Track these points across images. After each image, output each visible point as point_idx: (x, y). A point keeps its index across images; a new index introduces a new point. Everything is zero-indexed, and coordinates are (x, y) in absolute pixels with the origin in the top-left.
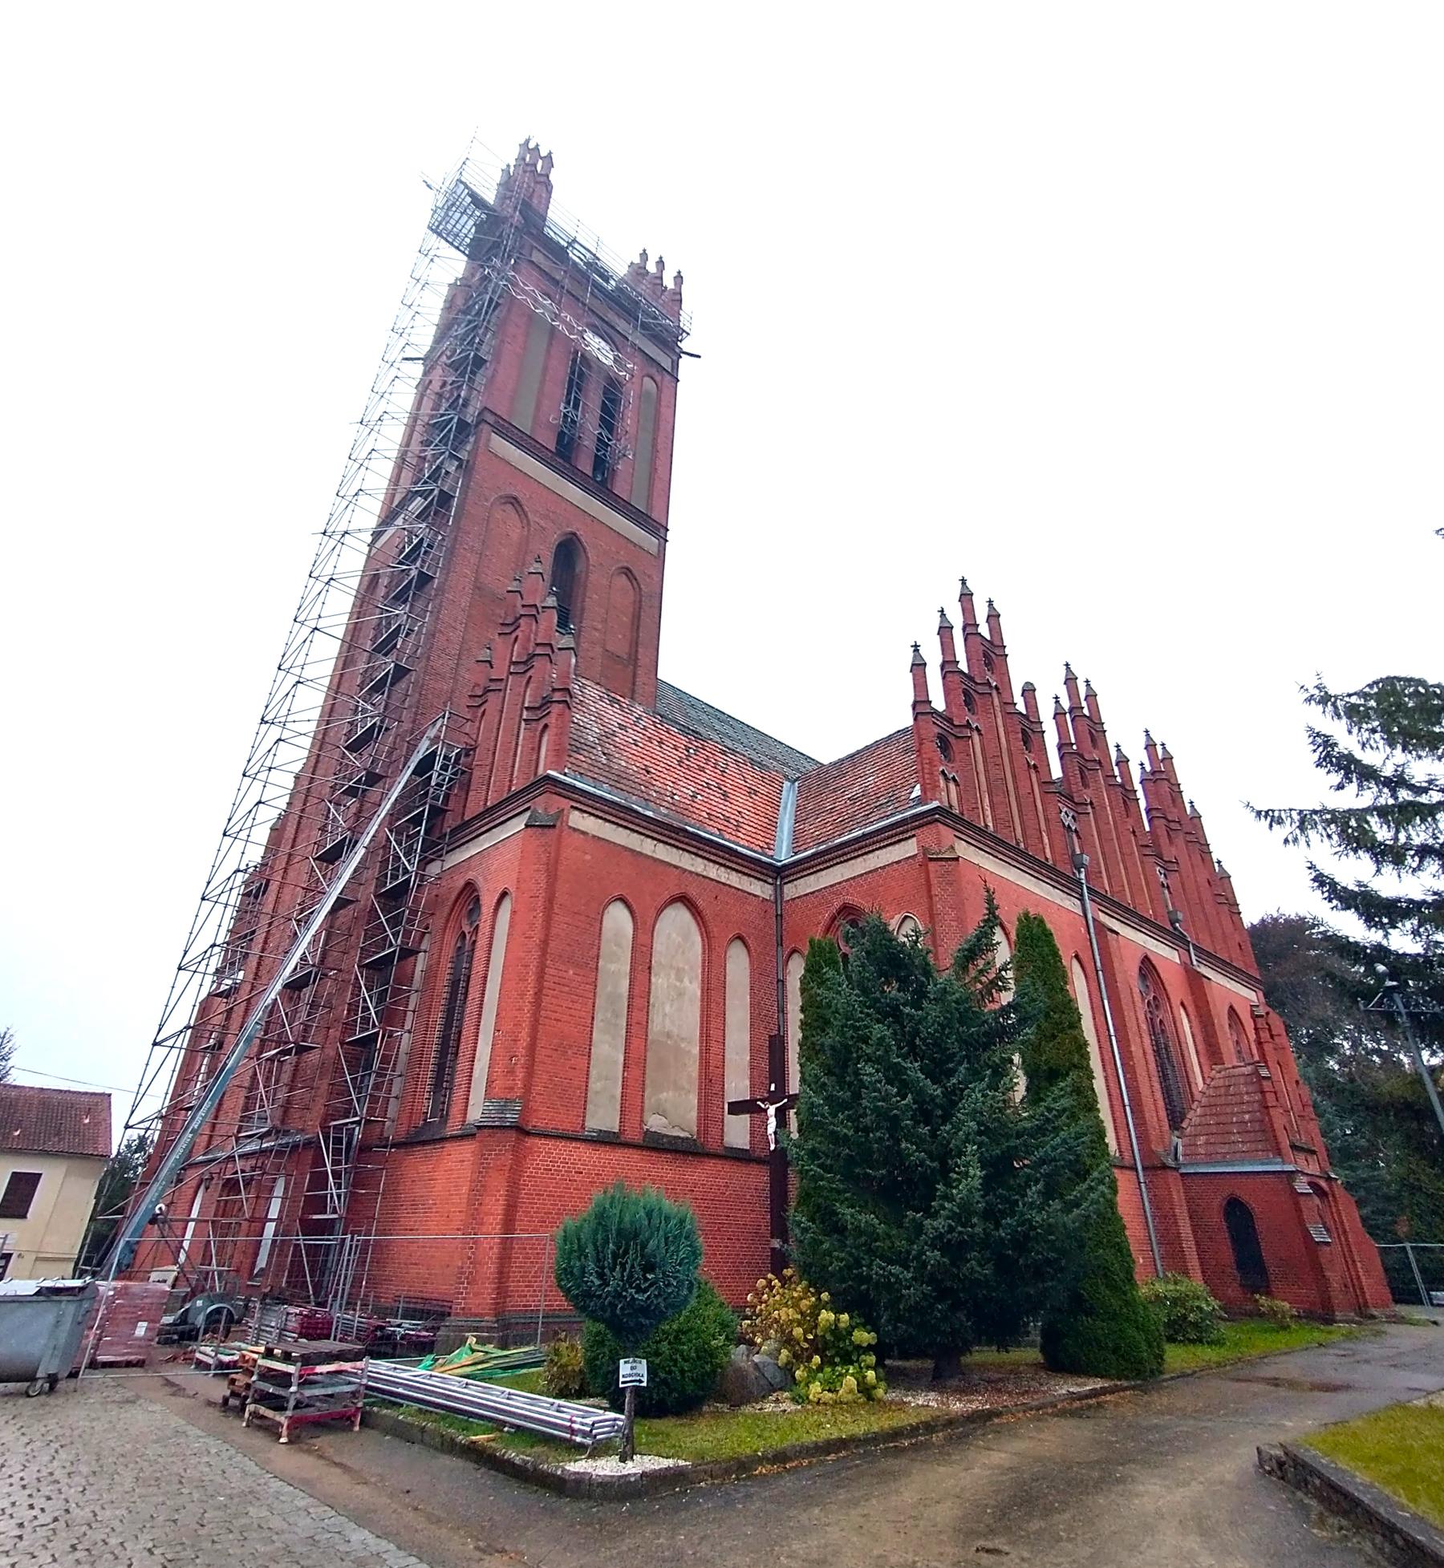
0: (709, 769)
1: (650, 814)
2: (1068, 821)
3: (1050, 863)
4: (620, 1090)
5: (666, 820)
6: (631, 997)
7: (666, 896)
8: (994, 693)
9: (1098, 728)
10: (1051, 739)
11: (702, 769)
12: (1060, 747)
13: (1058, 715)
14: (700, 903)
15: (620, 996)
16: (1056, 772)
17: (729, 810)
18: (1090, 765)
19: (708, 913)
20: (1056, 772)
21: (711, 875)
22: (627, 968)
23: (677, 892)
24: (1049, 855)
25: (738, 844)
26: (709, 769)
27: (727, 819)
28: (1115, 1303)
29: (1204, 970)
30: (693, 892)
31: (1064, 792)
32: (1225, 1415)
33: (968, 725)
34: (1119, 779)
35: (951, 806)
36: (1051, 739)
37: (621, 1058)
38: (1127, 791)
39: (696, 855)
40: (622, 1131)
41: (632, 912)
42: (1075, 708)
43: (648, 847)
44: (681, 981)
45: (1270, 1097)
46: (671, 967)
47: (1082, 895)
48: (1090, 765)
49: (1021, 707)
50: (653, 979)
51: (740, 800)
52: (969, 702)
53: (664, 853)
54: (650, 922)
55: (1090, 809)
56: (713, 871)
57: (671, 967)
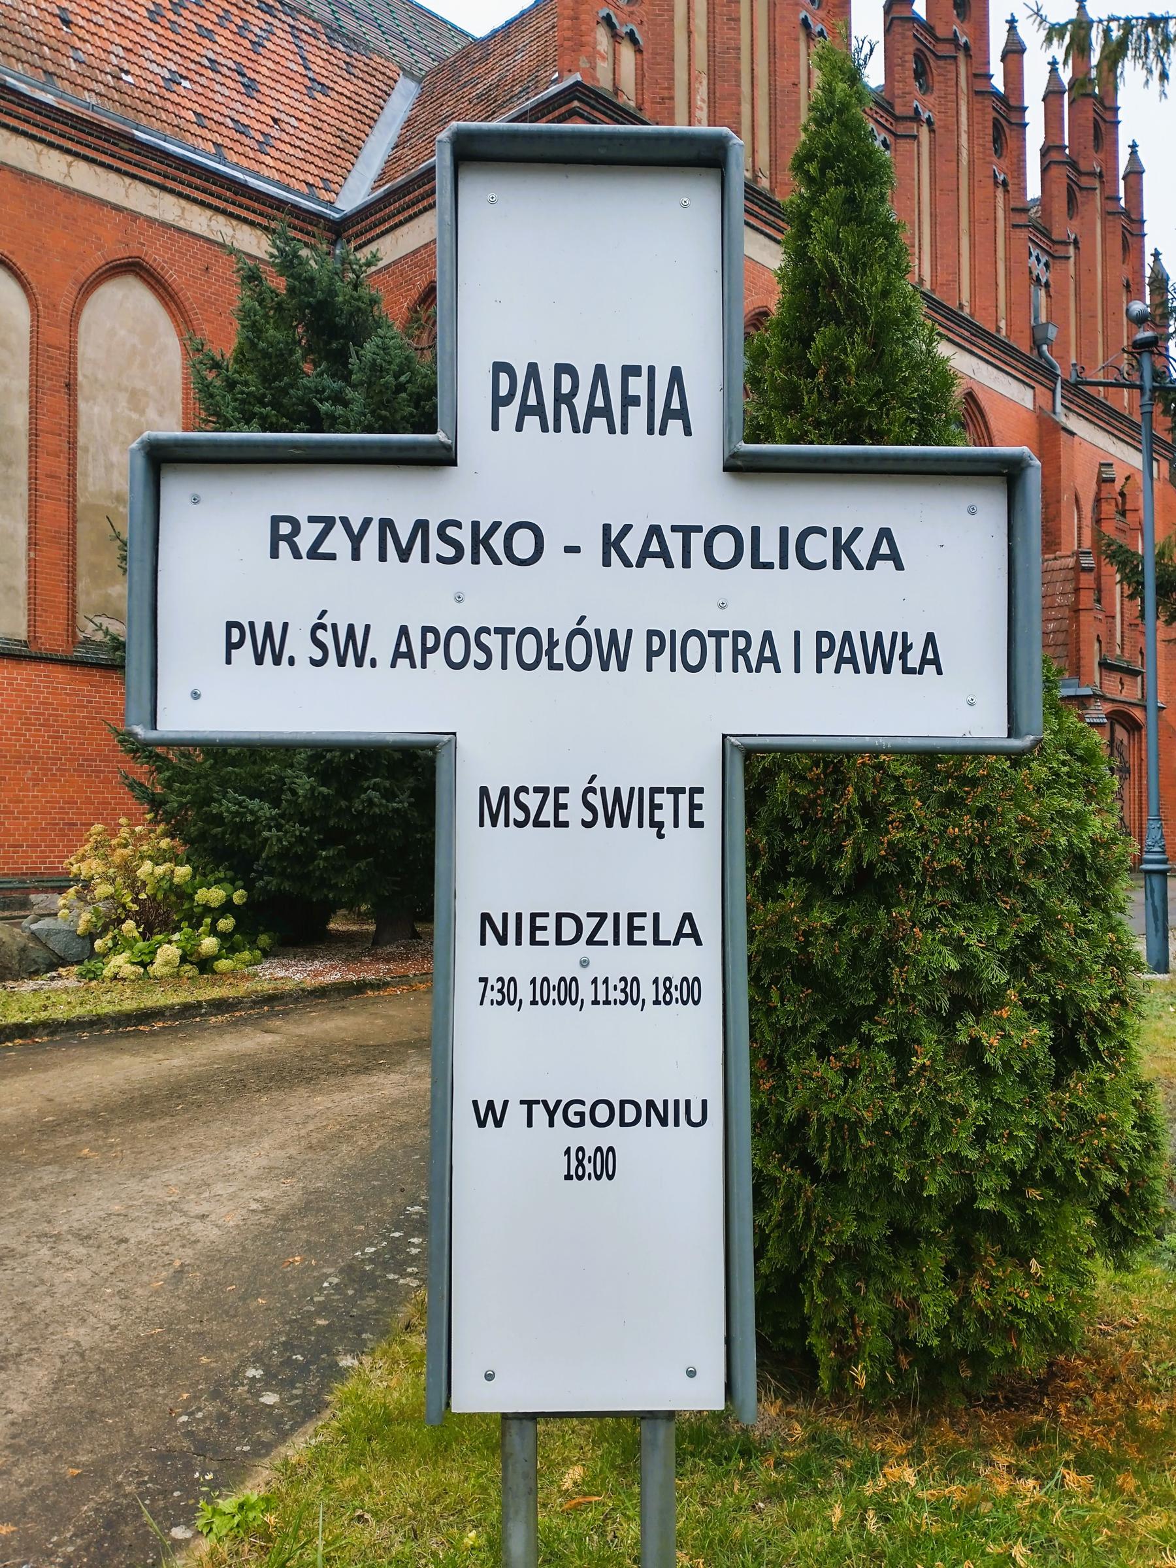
0: (223, 37)
1: (49, 99)
2: (1039, 270)
3: (966, 312)
4: (25, 578)
5: (87, 114)
6: (34, 433)
7: (97, 260)
8: (961, 56)
9: (1108, 116)
10: (1035, 137)
11: (208, 34)
12: (1045, 152)
13: (1052, 95)
14: (172, 276)
15: (12, 430)
16: (1034, 190)
17: (255, 115)
18: (1085, 181)
19: (189, 296)
20: (1034, 190)
21: (196, 229)
22: (22, 384)
23: (121, 253)
24: (1002, 324)
25: (257, 176)
26: (223, 37)
27: (243, 130)
28: (211, 878)
29: (1074, 423)
30: (156, 255)
31: (1038, 229)
32: (186, 1110)
33: (916, 117)
34: (1122, 203)
35: (616, 90)
36: (1035, 137)
37: (23, 531)
38: (1006, 116)
39: (163, 188)
40: (33, 638)
41: (25, 285)
42: (1080, 83)
43: (53, 166)
44: (142, 412)
45: (1087, 599)
46: (120, 388)
47: (1053, 391)
48: (1085, 181)
49: (998, 82)
50: (82, 405)
51: (284, 99)
52: (921, 73)
53: (86, 178)
54: (65, 304)
55: (1071, 249)
56: (199, 221)
57: (120, 388)
